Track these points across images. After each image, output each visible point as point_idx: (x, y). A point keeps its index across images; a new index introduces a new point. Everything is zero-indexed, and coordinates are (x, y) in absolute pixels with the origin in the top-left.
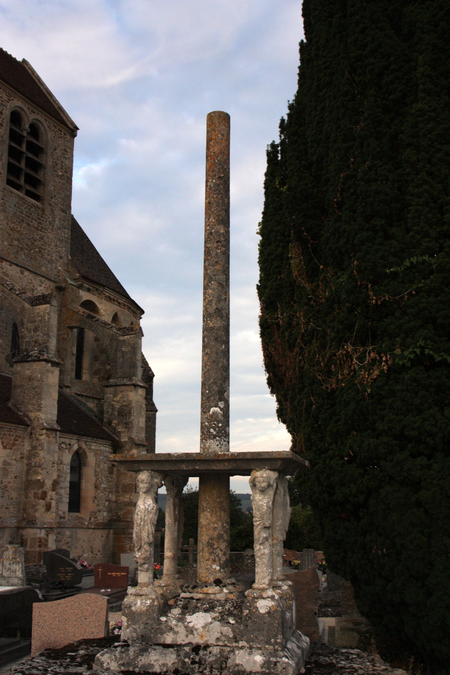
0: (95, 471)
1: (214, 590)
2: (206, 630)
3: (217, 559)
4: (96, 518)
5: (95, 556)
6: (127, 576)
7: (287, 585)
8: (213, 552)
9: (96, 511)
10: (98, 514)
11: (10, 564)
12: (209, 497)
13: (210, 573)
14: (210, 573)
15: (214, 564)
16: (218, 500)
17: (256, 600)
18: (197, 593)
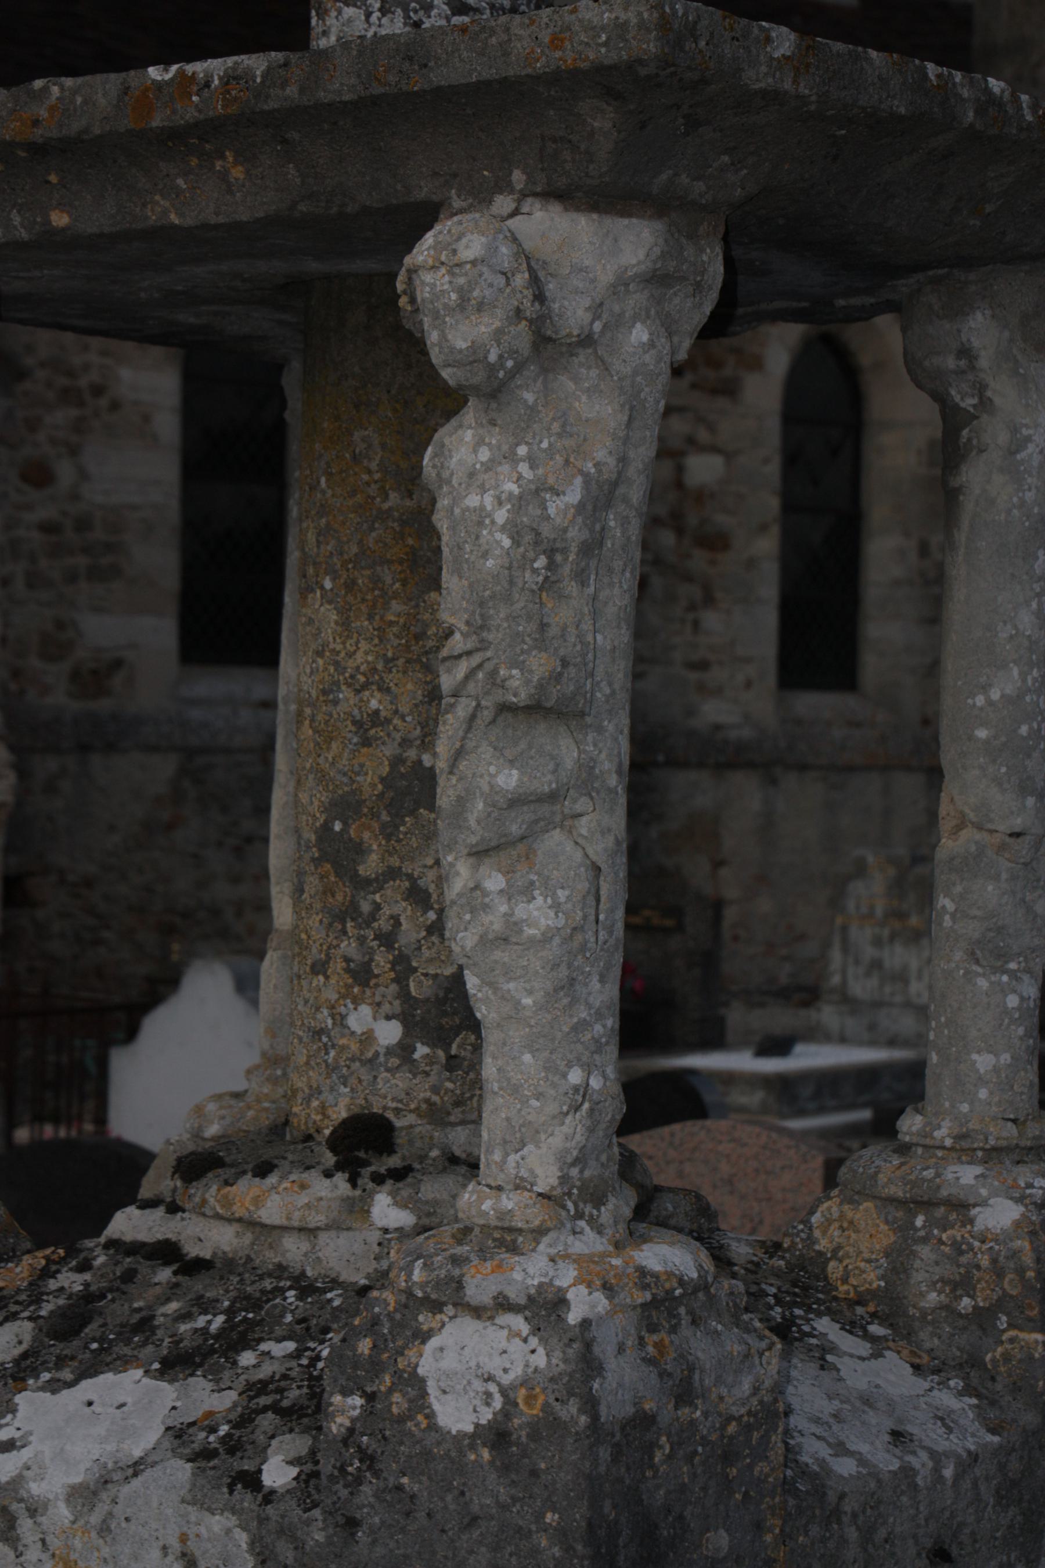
1: (303, 1199)
2: (95, 1519)
3: (382, 961)
7: (1020, 1200)
8: (350, 911)
11: (878, 942)
13: (332, 1069)
14: (332, 1069)
15: (356, 1002)
16: (394, 498)
17: (425, 1320)
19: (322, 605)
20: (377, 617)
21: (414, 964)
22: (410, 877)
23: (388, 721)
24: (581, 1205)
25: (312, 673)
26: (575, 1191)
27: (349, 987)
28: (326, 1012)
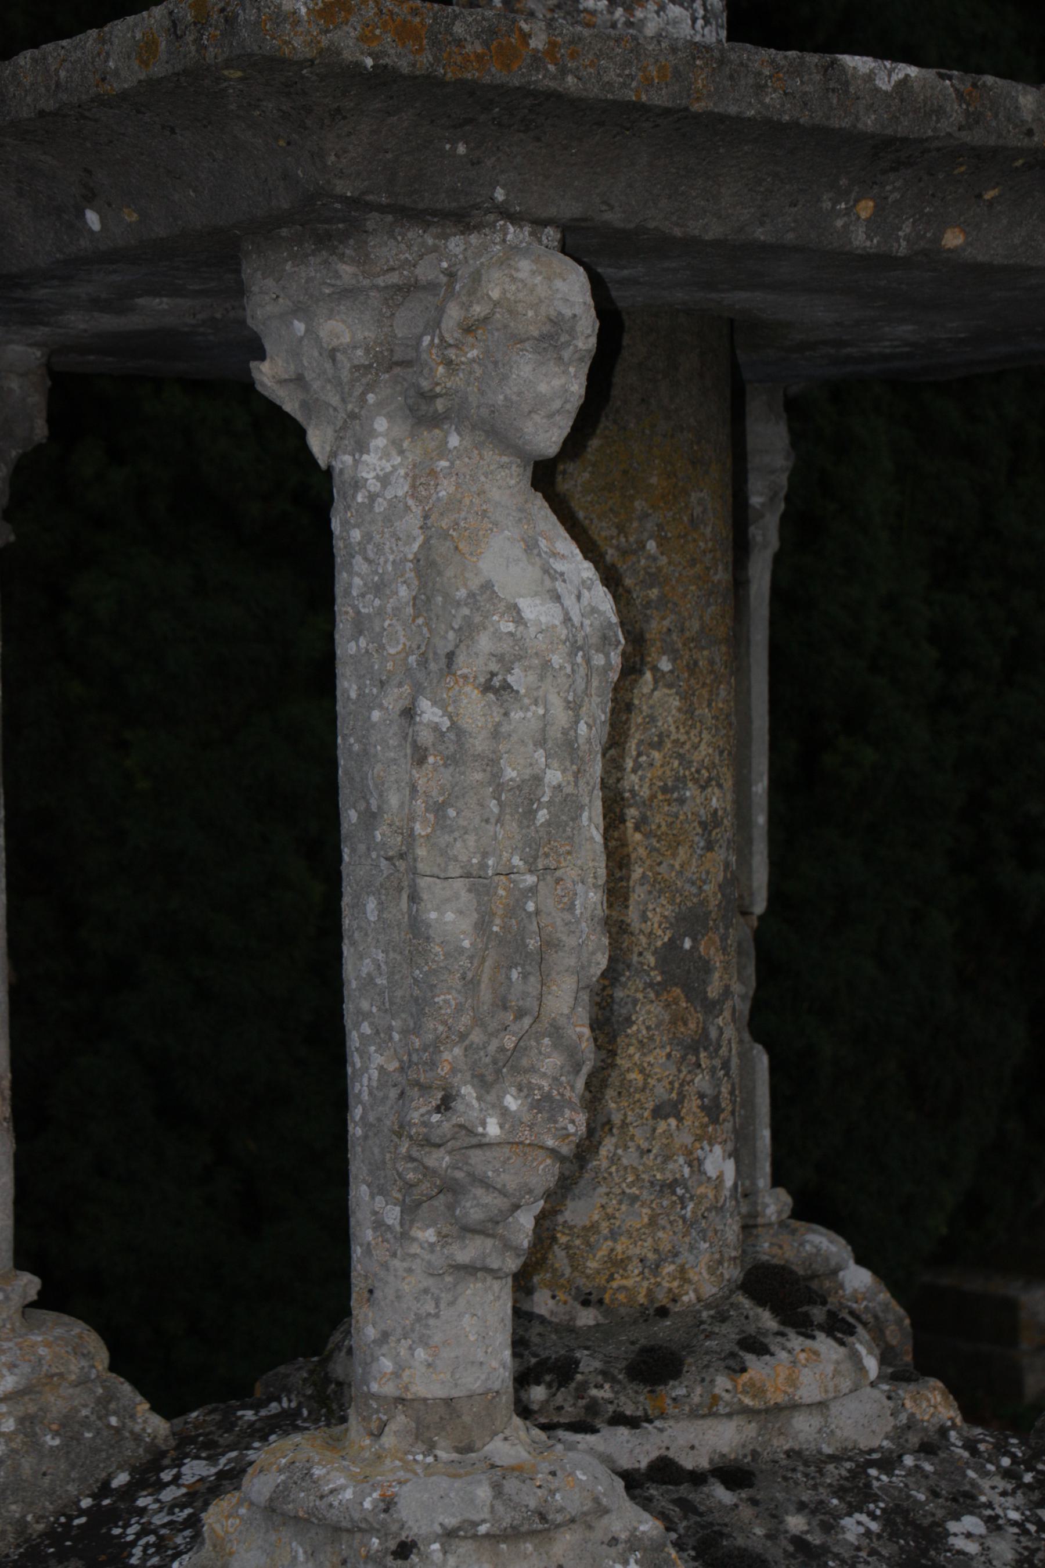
12: (662, 542)
18: (710, 1410)
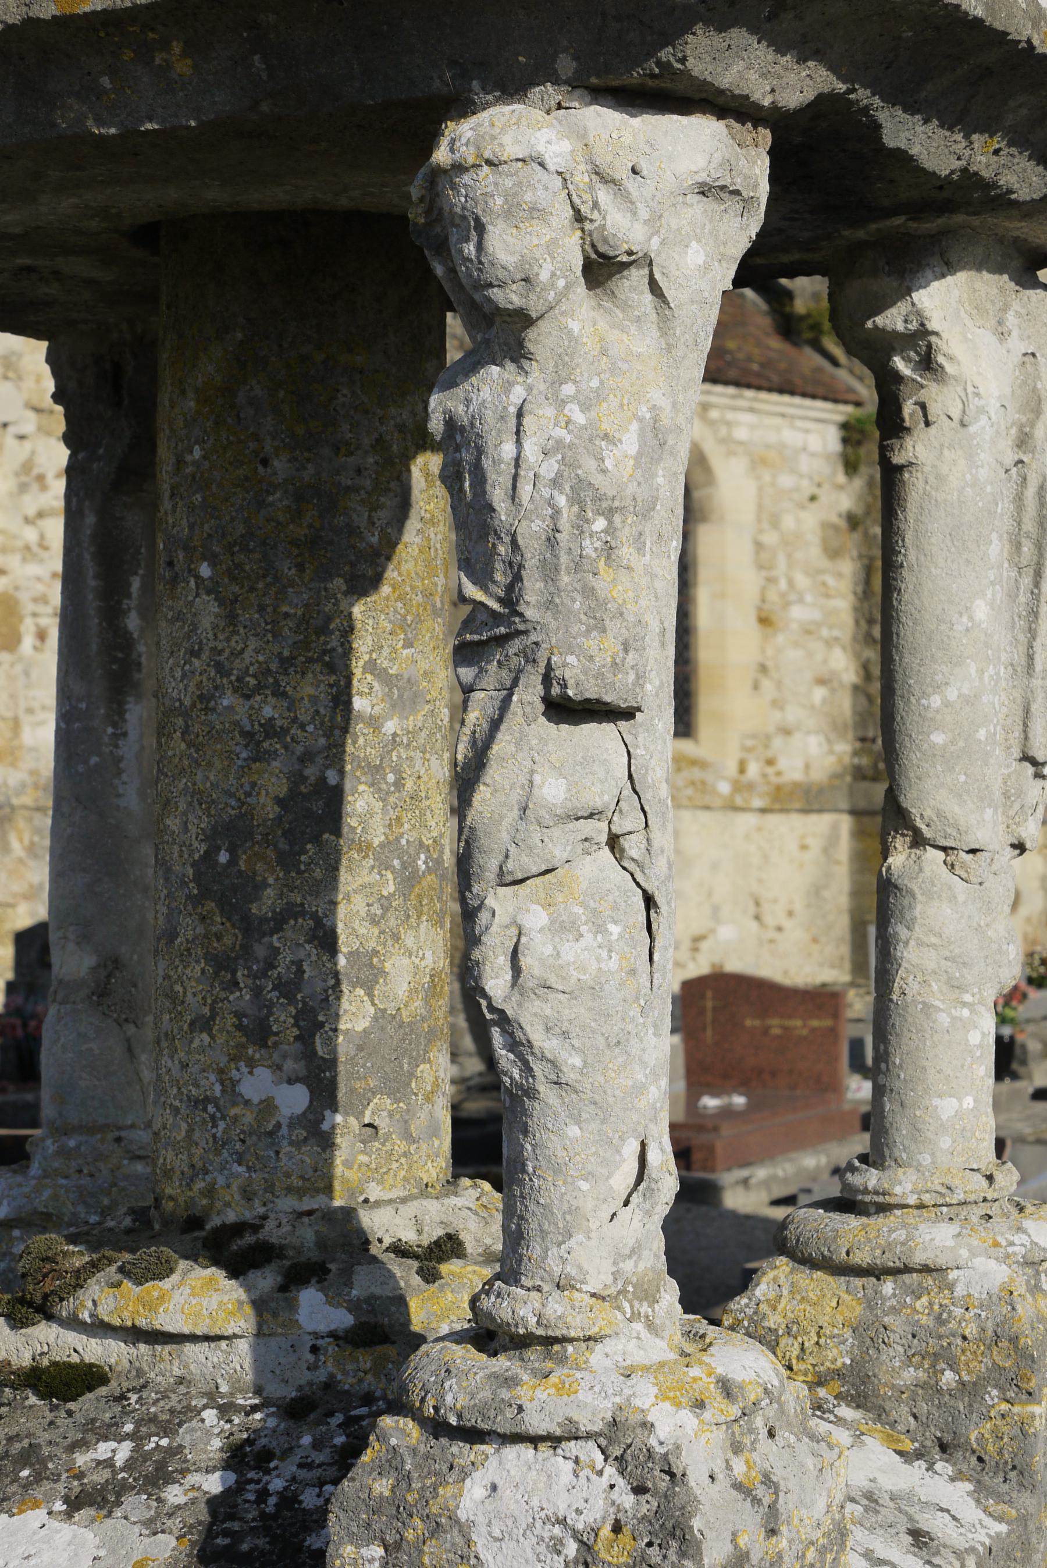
0: (759, 545)
3: (283, 1019)
4: (770, 762)
5: (772, 934)
6: (833, 1033)
9: (771, 729)
10: (778, 742)
19: (197, 595)
20: (269, 609)
21: (321, 1018)
22: (314, 916)
23: (285, 731)
24: (636, 1304)
25: (184, 676)
26: (630, 1289)
27: (241, 1047)
28: (212, 1077)
